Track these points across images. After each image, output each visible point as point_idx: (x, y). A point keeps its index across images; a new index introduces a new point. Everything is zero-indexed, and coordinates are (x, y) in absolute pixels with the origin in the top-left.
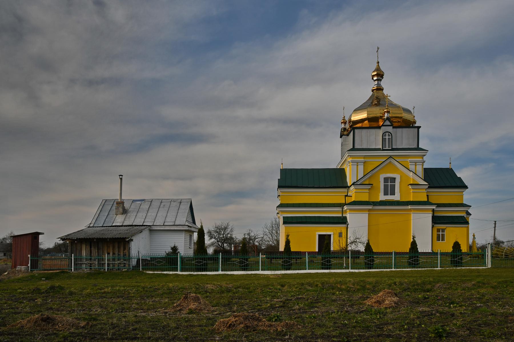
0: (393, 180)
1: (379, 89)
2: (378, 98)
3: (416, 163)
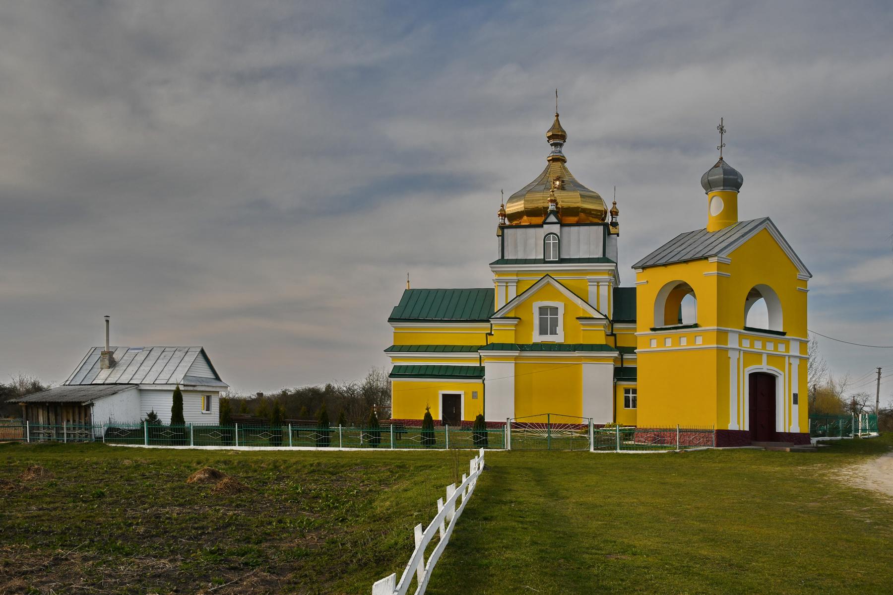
0: (555, 310)
1: (559, 159)
3: (598, 282)
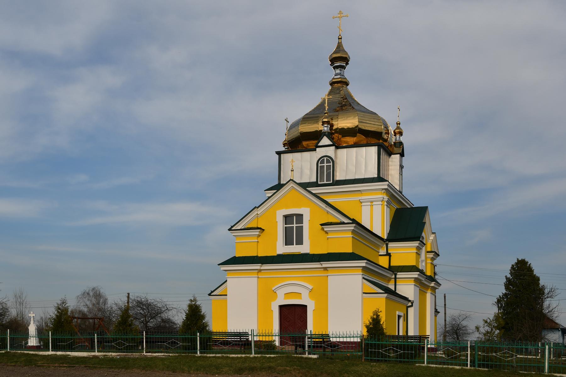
0: (300, 217)
2: (341, 101)
3: (372, 202)
